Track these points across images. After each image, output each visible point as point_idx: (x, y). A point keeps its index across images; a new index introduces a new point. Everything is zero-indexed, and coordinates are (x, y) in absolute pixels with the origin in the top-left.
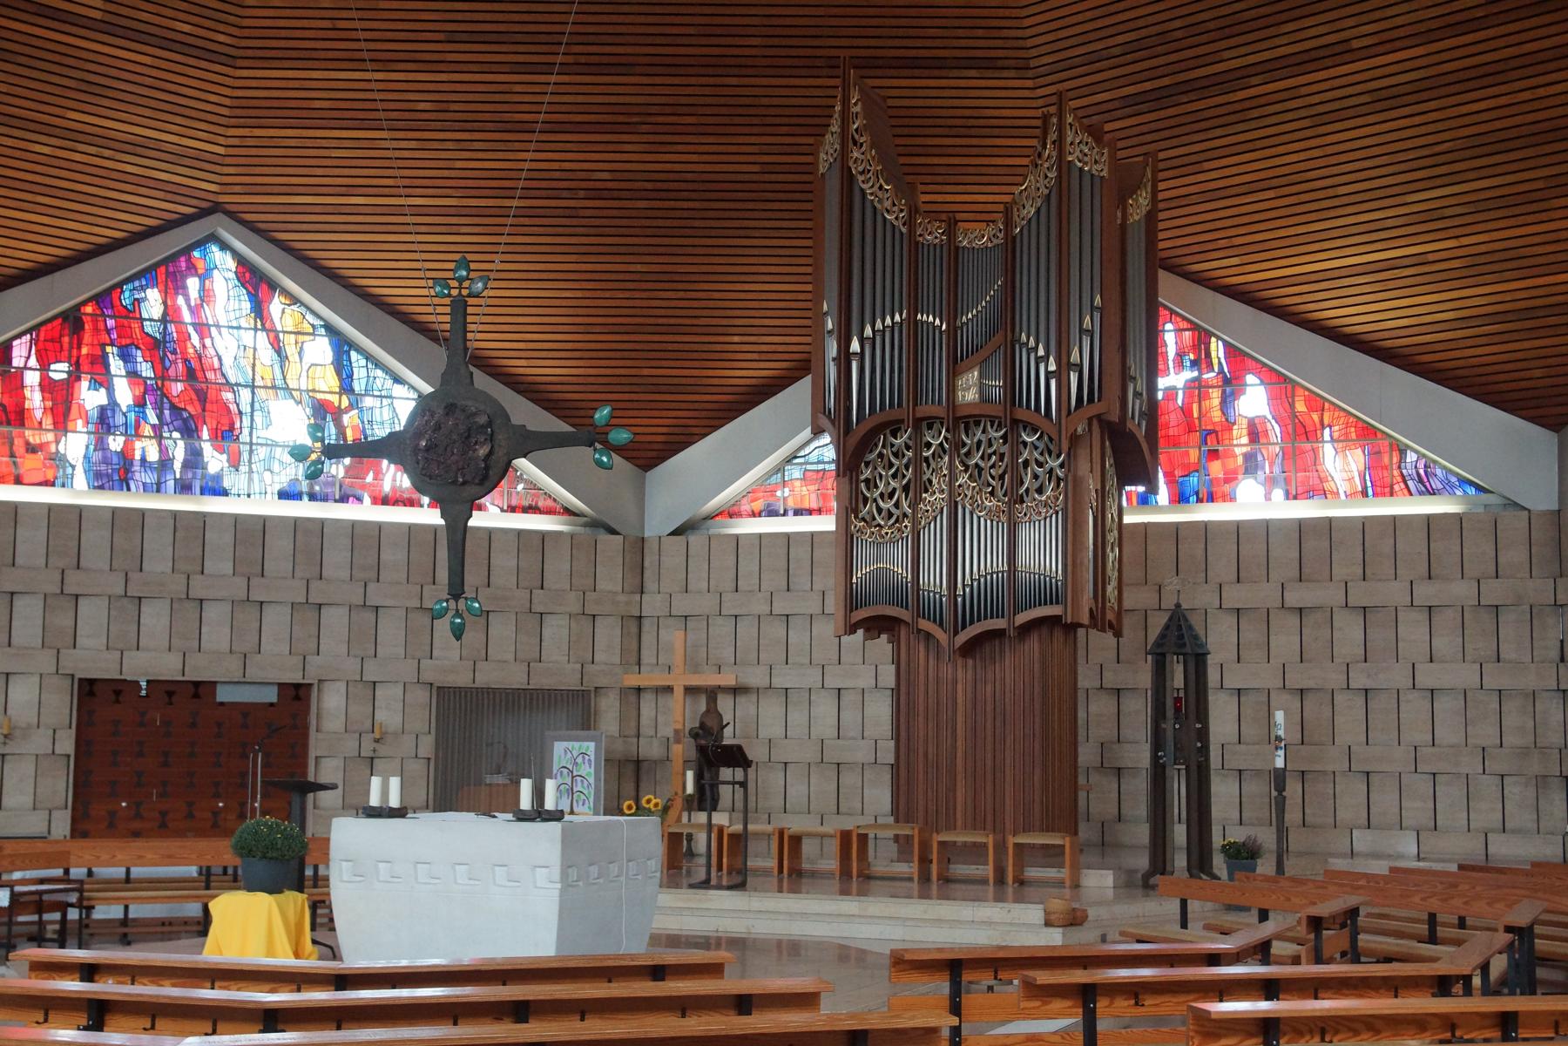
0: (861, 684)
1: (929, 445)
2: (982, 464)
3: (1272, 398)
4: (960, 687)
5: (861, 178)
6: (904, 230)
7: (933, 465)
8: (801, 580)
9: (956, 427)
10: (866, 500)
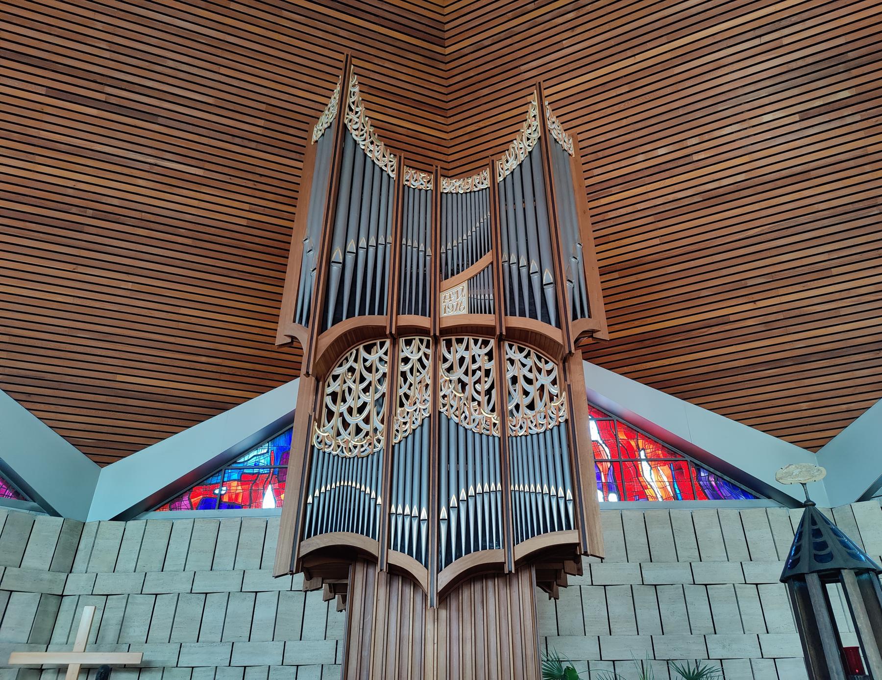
0: (268, 661)
2: (465, 379)
5: (354, 133)
6: (392, 175)
7: (410, 379)
8: (225, 560)
9: (436, 341)
10: (330, 414)
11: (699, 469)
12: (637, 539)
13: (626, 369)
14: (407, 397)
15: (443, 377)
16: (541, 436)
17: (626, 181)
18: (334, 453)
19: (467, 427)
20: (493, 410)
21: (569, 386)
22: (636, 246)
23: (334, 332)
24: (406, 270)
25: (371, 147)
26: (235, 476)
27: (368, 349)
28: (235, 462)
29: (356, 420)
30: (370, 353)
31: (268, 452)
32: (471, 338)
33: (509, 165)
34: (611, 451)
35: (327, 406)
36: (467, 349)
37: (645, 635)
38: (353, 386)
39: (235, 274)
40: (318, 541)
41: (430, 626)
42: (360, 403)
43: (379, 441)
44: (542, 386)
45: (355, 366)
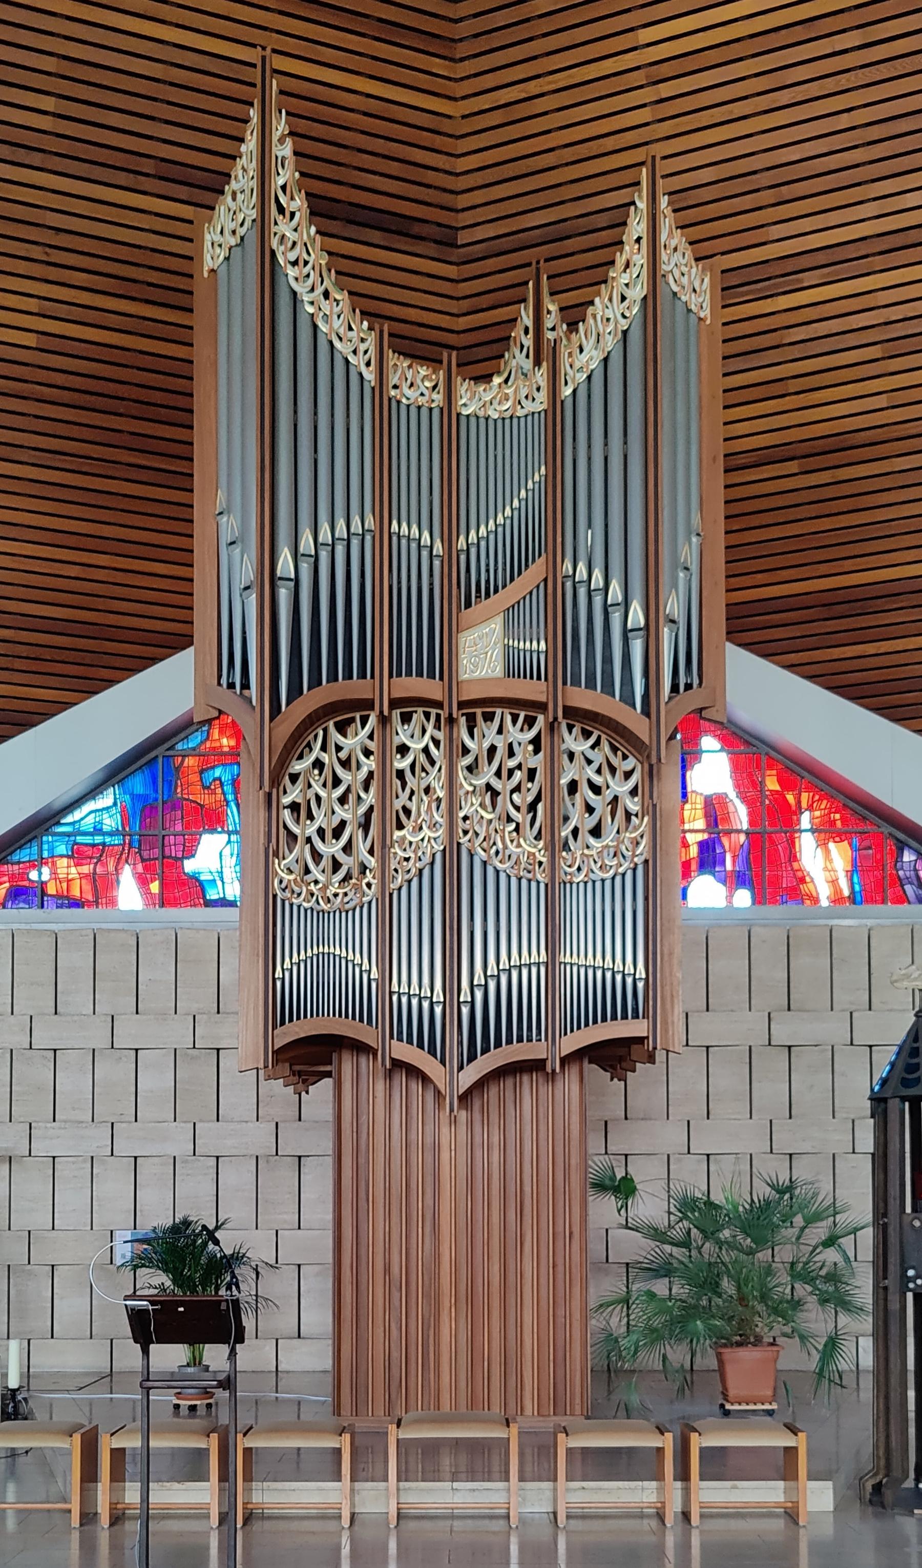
0: (172, 1150)
1: (403, 750)
2: (497, 784)
3: (736, 767)
4: (445, 1156)
5: (292, 272)
7: (411, 782)
8: (77, 999)
11: (901, 846)
12: (771, 972)
13: (793, 658)
14: (407, 812)
15: (465, 783)
16: (608, 884)
17: (835, 260)
18: (305, 905)
19: (500, 866)
20: (538, 837)
21: (654, 806)
22: (839, 410)
23: (295, 714)
24: (399, 582)
25: (326, 306)
26: (62, 849)
27: (342, 728)
28: (58, 823)
29: (331, 849)
30: (345, 735)
31: (115, 804)
32: (507, 711)
33: (584, 357)
34: (750, 814)
35: (285, 827)
36: (500, 731)
37: (761, 1119)
38: (323, 794)
39: (24, 456)
40: (297, 1029)
41: (445, 1130)
42: (335, 822)
43: (369, 885)
44: (616, 798)
45: (325, 758)
